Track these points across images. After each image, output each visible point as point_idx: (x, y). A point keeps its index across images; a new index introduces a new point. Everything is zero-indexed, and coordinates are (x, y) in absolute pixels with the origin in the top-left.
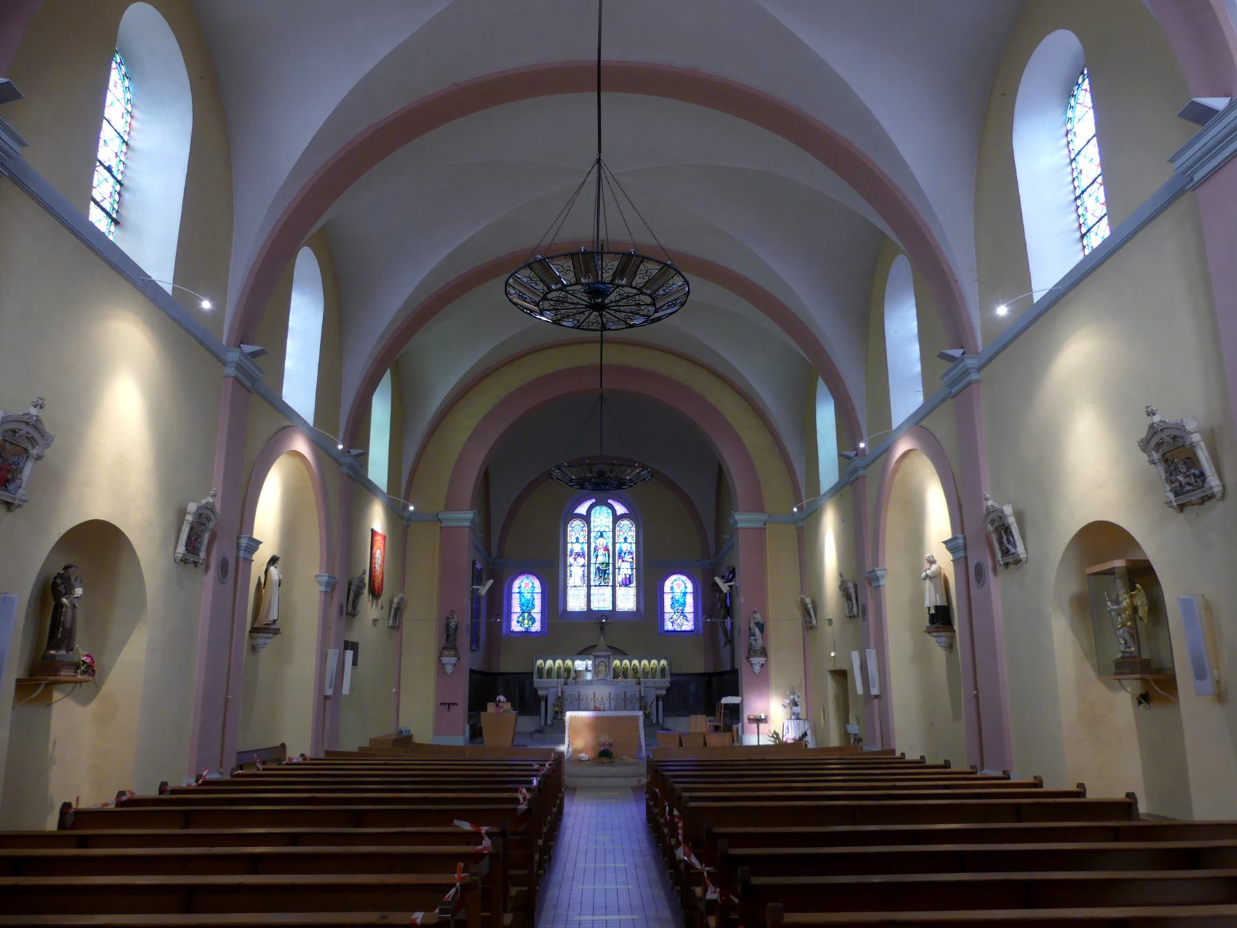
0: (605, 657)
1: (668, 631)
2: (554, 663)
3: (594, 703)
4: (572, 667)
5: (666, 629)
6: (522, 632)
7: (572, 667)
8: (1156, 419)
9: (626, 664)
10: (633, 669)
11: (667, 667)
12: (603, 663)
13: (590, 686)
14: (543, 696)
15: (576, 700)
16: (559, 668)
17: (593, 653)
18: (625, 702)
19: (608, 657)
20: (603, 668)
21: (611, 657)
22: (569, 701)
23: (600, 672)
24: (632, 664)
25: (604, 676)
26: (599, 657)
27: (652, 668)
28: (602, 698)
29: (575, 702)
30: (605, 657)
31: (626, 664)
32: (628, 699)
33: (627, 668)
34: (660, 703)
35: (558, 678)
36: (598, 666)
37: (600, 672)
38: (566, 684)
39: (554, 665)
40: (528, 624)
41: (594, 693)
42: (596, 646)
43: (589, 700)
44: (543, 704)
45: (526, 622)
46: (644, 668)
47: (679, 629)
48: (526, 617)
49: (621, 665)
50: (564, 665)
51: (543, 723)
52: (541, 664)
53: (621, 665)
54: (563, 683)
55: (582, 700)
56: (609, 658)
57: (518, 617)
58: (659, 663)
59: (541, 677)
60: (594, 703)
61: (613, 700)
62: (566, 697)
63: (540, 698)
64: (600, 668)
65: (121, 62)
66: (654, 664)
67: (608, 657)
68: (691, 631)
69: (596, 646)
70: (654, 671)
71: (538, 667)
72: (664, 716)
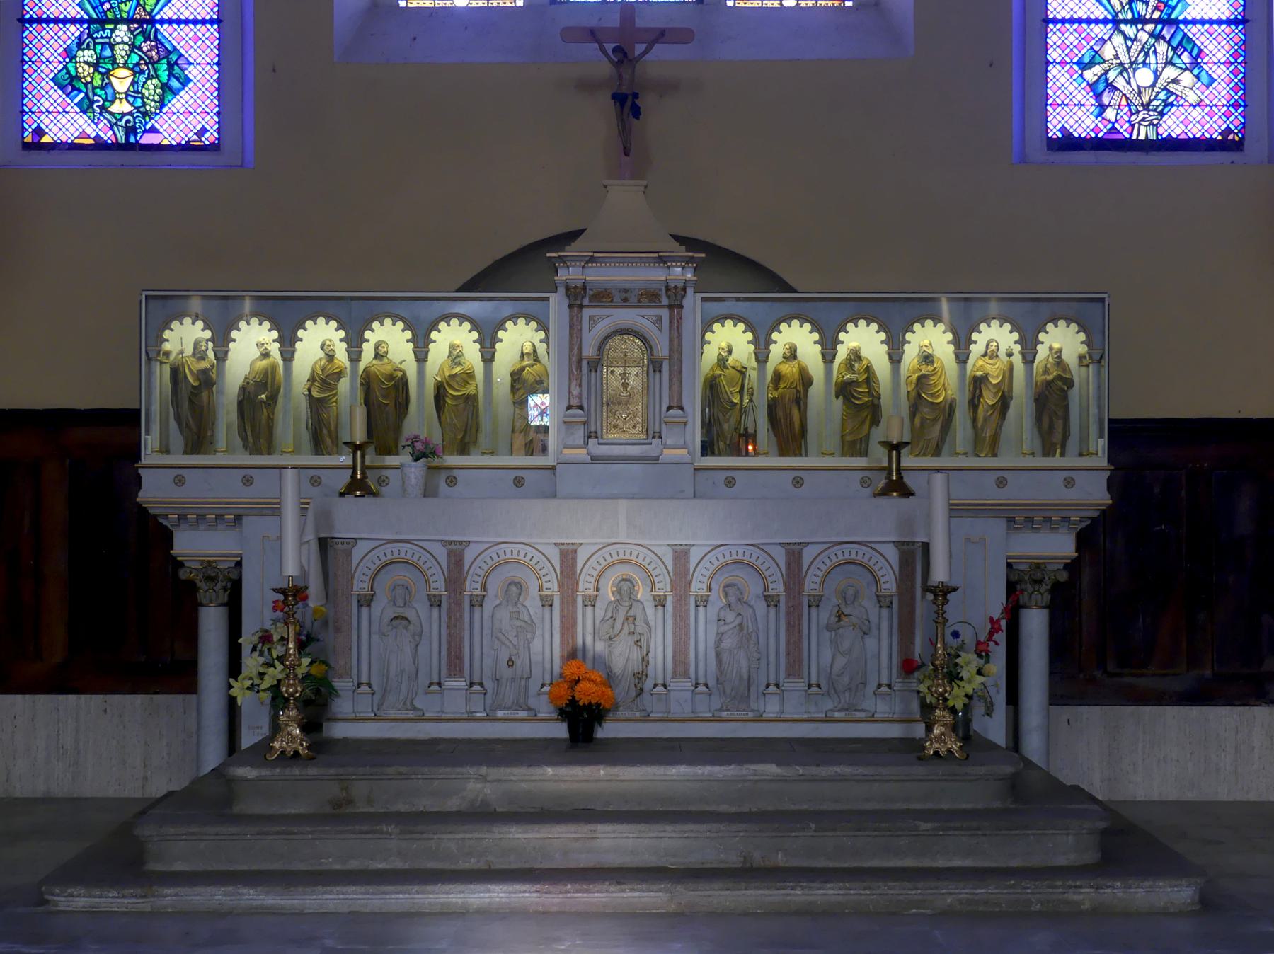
0: (649, 297)
1: (1069, 143)
2: (288, 342)
3: (568, 625)
4: (411, 368)
5: (1054, 132)
6: (100, 145)
7: (411, 368)
8: (202, 585)
9: (792, 355)
10: (844, 390)
11: (1077, 373)
12: (634, 347)
13: (537, 508)
14: (210, 571)
15: (435, 602)
16: (325, 379)
17: (563, 275)
18: (794, 626)
19: (674, 296)
20: (635, 378)
21: (692, 301)
22: (382, 608)
23: (614, 403)
24: (842, 353)
25: (636, 433)
26: (603, 297)
27: (979, 382)
28: (626, 590)
29: (419, 610)
30: (649, 297)
31: (792, 355)
32: (815, 602)
33: (806, 380)
34: (1035, 623)
35: (318, 447)
36: (595, 365)
37: (614, 403)
38: (358, 486)
39: (288, 355)
40: (134, 93)
41: (568, 556)
42: (573, 236)
43: (532, 603)
44: (212, 621)
45: (121, 80)
46: (922, 381)
47: (1142, 134)
48: (121, 51)
49: (762, 359)
50: (355, 357)
51: (213, 754)
52: (199, 354)
53: (762, 359)
54: (344, 478)
55: (477, 602)
56: (676, 306)
57: (69, 55)
58: (1029, 346)
59: (199, 440)
60: (568, 625)
61: (704, 601)
62: (360, 585)
63: (191, 586)
64: (611, 379)
65: (729, 445)
66: (990, 354)
67: (674, 296)
68: (1225, 145)
69: (573, 236)
70: (989, 399)
71: (712, 385)
72: (1057, 697)
